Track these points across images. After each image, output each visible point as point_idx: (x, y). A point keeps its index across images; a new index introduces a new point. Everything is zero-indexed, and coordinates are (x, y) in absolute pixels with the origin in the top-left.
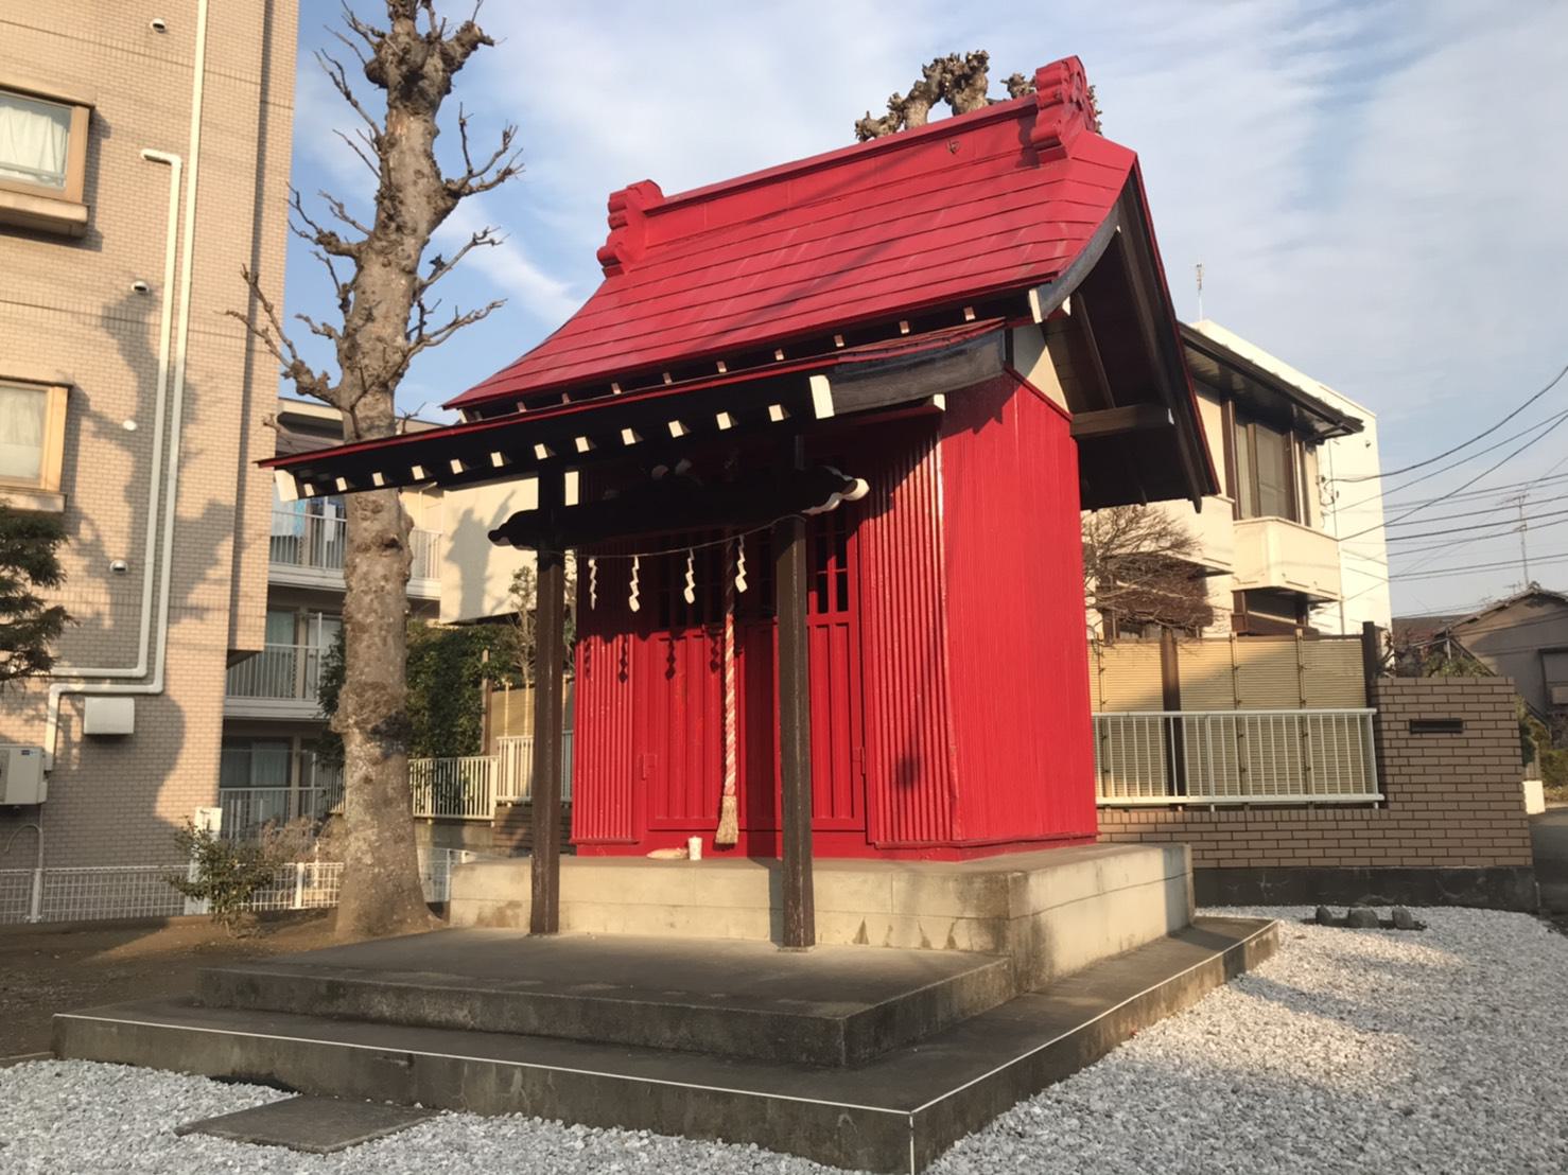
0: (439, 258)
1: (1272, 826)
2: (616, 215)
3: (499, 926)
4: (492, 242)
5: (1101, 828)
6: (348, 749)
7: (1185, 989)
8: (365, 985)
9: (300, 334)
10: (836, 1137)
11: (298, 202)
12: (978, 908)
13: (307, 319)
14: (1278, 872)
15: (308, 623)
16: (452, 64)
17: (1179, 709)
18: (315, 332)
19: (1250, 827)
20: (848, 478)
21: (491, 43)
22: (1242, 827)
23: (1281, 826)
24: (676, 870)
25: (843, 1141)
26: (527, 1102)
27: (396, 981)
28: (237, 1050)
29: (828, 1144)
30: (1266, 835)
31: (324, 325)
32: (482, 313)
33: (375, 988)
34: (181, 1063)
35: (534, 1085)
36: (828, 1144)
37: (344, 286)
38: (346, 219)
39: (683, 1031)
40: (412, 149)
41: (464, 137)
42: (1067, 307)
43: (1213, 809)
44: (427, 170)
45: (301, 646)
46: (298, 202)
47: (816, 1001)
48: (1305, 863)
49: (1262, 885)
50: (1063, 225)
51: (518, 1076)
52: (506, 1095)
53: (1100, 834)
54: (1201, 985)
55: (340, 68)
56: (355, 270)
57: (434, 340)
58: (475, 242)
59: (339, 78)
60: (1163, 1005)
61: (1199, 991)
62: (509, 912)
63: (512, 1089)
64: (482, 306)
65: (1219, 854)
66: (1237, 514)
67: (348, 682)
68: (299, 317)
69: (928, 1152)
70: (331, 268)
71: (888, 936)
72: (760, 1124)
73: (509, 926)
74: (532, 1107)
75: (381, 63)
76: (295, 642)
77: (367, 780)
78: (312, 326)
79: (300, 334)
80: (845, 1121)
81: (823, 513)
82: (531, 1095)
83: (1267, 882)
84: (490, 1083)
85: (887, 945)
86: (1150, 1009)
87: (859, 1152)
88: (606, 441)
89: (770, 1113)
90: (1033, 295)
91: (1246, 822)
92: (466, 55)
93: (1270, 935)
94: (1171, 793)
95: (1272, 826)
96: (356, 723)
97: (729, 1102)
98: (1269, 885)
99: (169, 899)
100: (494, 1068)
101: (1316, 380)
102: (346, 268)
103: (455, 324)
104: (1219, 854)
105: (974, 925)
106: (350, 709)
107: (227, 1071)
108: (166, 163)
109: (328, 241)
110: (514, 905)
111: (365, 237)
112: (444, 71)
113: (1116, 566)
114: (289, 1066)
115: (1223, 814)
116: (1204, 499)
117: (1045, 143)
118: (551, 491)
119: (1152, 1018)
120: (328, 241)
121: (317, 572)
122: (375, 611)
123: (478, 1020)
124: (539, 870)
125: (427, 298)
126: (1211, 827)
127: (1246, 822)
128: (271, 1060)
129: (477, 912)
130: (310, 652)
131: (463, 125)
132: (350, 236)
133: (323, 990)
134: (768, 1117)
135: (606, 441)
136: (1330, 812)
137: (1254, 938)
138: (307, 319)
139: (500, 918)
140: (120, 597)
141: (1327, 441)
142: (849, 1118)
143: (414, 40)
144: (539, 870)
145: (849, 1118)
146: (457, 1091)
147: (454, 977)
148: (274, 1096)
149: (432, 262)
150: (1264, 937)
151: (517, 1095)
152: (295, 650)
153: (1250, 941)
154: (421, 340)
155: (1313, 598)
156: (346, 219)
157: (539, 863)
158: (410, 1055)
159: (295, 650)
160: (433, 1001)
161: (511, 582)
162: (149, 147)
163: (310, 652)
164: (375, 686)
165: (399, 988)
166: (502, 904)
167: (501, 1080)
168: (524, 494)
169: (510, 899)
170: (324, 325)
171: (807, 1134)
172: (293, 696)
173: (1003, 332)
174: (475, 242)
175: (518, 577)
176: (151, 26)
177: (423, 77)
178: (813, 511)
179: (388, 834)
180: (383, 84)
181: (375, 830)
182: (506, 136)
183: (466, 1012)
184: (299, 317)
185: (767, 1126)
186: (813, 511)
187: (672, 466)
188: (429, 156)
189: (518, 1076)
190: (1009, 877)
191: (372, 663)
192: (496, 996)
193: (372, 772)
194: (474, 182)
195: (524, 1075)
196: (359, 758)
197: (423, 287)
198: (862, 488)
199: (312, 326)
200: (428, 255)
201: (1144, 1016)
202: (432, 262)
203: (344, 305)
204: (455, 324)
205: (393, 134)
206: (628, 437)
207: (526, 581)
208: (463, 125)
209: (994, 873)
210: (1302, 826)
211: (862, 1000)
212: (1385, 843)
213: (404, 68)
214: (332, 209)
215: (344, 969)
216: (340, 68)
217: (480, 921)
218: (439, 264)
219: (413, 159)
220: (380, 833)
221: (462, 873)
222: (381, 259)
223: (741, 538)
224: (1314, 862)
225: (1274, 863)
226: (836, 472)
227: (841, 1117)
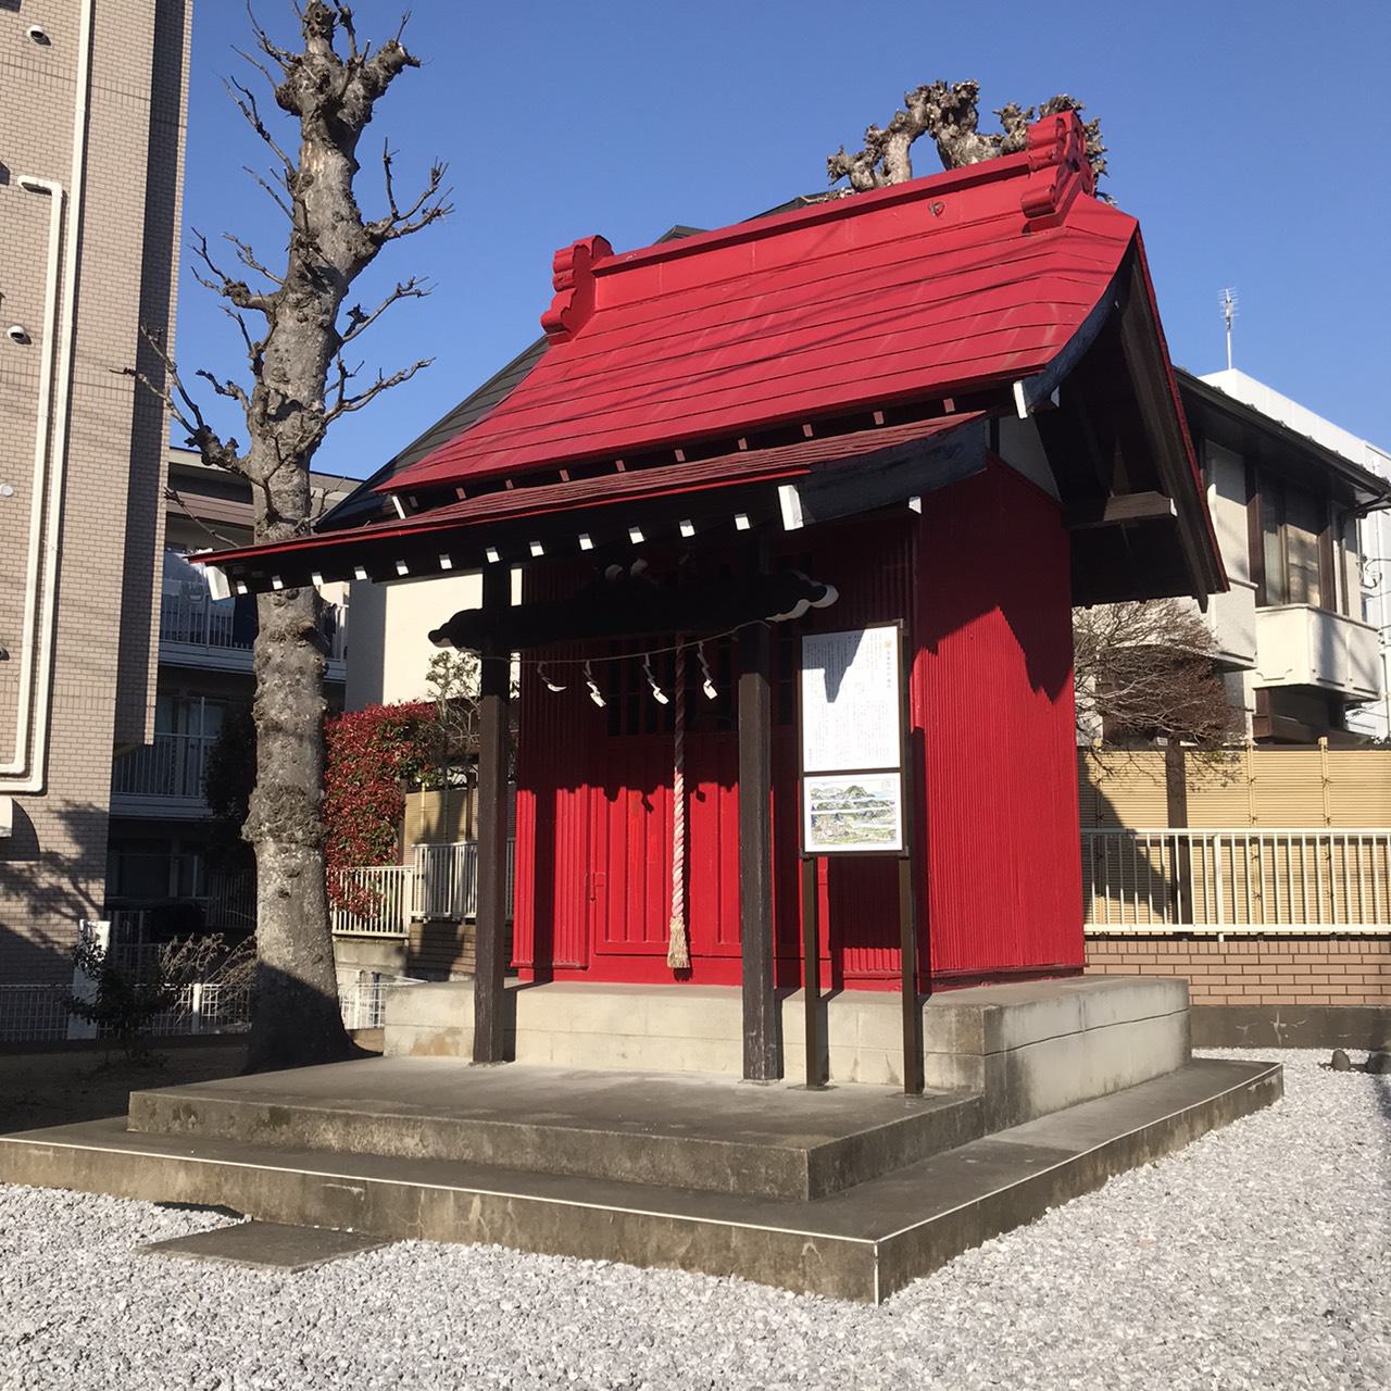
0: (357, 309)
1: (1289, 959)
2: (561, 274)
3: (437, 1054)
4: (419, 295)
5: (1092, 959)
6: (260, 860)
7: (1172, 1133)
8: (309, 1112)
9: (201, 391)
10: (800, 1266)
11: (204, 249)
12: (949, 1043)
13: (210, 377)
14: (1291, 1012)
15: (188, 709)
16: (374, 90)
17: (1185, 826)
18: (220, 390)
19: (1264, 960)
20: (815, 584)
21: (417, 65)
22: (1254, 959)
23: (1298, 959)
24: (628, 997)
25: (807, 1269)
26: (486, 1230)
27: (344, 1108)
28: (182, 1174)
29: (793, 1272)
30: (1281, 969)
31: (229, 383)
32: (407, 374)
33: (321, 1115)
34: (123, 1189)
35: (493, 1212)
36: (793, 1272)
37: (257, 344)
38: (253, 264)
39: (644, 1161)
40: (330, 188)
41: (389, 176)
42: (1055, 398)
43: (1221, 938)
44: (345, 211)
45: (181, 734)
46: (204, 249)
47: (781, 1133)
48: (1324, 1001)
49: (1276, 1025)
50: (1053, 306)
51: (476, 1203)
52: (465, 1223)
53: (1088, 965)
54: (1192, 1129)
55: (251, 97)
56: (268, 326)
57: (354, 405)
58: (399, 294)
59: (250, 108)
60: (1147, 1149)
61: (1188, 1136)
62: (448, 1040)
63: (471, 1216)
64: (407, 365)
65: (1228, 990)
66: (1261, 601)
67: (260, 784)
68: (201, 373)
69: (893, 1281)
70: (243, 325)
71: (854, 1069)
72: (725, 1252)
73: (447, 1054)
74: (491, 1234)
75: (293, 87)
76: (175, 730)
77: (283, 894)
78: (216, 385)
79: (201, 391)
80: (809, 1249)
81: (789, 620)
82: (491, 1222)
83: (1281, 1022)
84: (448, 1210)
85: (853, 1080)
86: (1131, 1152)
87: (824, 1280)
88: (562, 547)
89: (735, 1241)
90: (1018, 388)
91: (1259, 954)
92: (388, 79)
93: (1274, 1079)
94: (1175, 921)
95: (1289, 959)
96: (270, 830)
97: (692, 1231)
98: (1284, 1025)
99: (54, 1021)
100: (452, 1194)
101: (1362, 438)
102: (257, 323)
103: (380, 387)
104: (1228, 990)
105: (946, 1059)
106: (262, 815)
107: (171, 1197)
108: (47, 192)
109: (237, 292)
110: (454, 1031)
111: (278, 288)
112: (365, 98)
113: (1119, 666)
114: (237, 1191)
115: (1233, 944)
116: (1212, 597)
117: (1038, 210)
118: (496, 587)
119: (1134, 1161)
120: (237, 292)
121: (201, 650)
122: (290, 708)
123: (430, 1149)
124: (483, 995)
125: (347, 353)
126: (1220, 959)
127: (1259, 954)
128: (218, 1184)
129: (413, 1039)
130: (191, 742)
131: (388, 161)
132: (262, 287)
133: (266, 1116)
134: (733, 1246)
135: (562, 547)
136: (1354, 944)
137: (1255, 1082)
138: (210, 377)
139: (439, 1045)
140: (70, 705)
141: (1369, 514)
142: (813, 1247)
143: (332, 62)
144: (483, 995)
145: (813, 1247)
146: (412, 1218)
147: (402, 1105)
148: (226, 1221)
149: (349, 314)
150: (1267, 1081)
151: (475, 1222)
152: (175, 738)
153: (1250, 1084)
154: (342, 405)
155: (1351, 698)
156: (253, 264)
157: (483, 988)
158: (365, 1181)
159: (175, 738)
160: (382, 1129)
161: (427, 668)
162: (27, 174)
163: (191, 742)
164: (288, 790)
165: (347, 1115)
166: (441, 1031)
167: (459, 1207)
168: (467, 592)
169: (449, 1025)
170: (229, 383)
171: (772, 1262)
172: (172, 792)
173: (987, 422)
174: (399, 294)
175: (435, 663)
176: (29, 34)
177: (342, 106)
178: (779, 617)
179: (304, 953)
180: (297, 112)
181: (291, 949)
182: (436, 173)
183: (417, 1139)
184: (201, 373)
185: (731, 1255)
186: (779, 617)
187: (627, 565)
188: (348, 195)
189: (476, 1203)
190: (982, 1010)
191: (287, 765)
192: (447, 1124)
193: (288, 885)
194: (400, 226)
195: (483, 1202)
196: (273, 869)
197: (341, 342)
198: (831, 597)
199: (216, 385)
200: (347, 304)
201: (1125, 1160)
202: (349, 314)
203: (258, 367)
204: (380, 387)
205: (308, 170)
206: (586, 544)
207: (446, 667)
208: (388, 161)
209: (967, 1006)
210: (1152, 959)
211: (827, 1133)
212: (1278, 980)
213: (322, 97)
214: (240, 255)
215: (284, 1095)
216: (251, 97)
217: (419, 1048)
218: (358, 315)
219: (331, 200)
220: (295, 952)
221: (397, 997)
222: (296, 313)
223: (701, 644)
224: (1336, 1001)
225: (1290, 1001)
226: (804, 577)
227: (806, 1246)
